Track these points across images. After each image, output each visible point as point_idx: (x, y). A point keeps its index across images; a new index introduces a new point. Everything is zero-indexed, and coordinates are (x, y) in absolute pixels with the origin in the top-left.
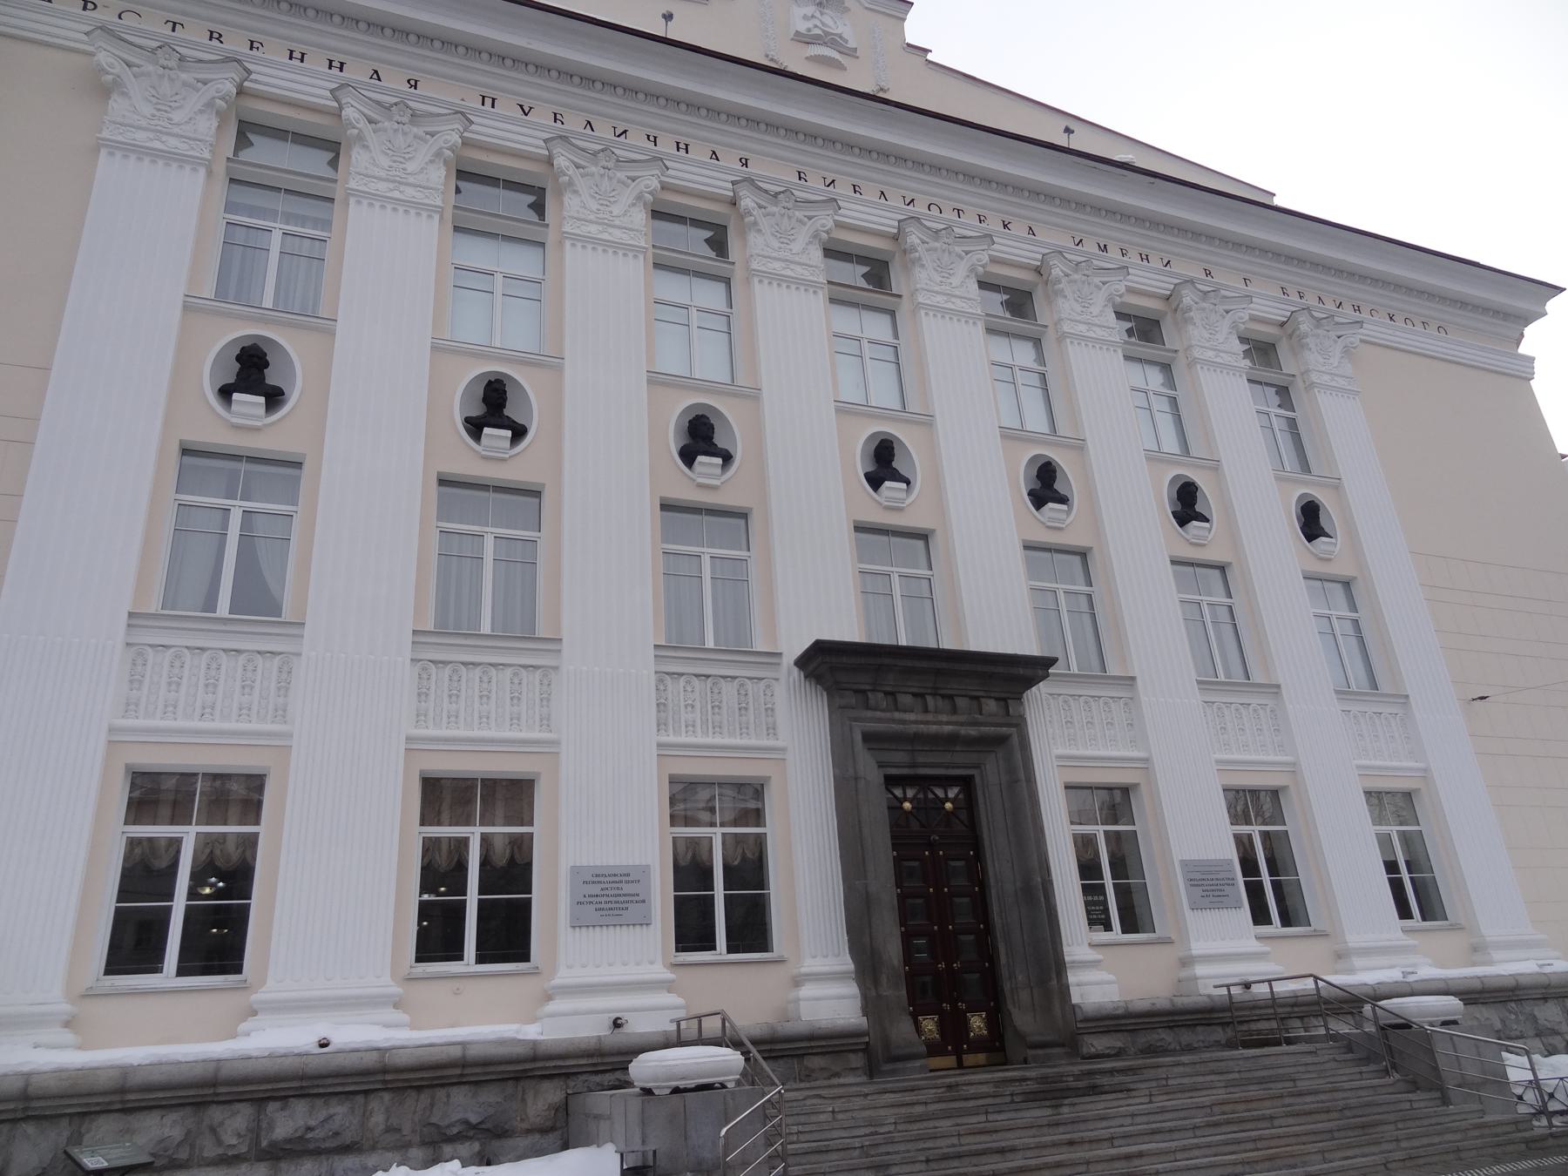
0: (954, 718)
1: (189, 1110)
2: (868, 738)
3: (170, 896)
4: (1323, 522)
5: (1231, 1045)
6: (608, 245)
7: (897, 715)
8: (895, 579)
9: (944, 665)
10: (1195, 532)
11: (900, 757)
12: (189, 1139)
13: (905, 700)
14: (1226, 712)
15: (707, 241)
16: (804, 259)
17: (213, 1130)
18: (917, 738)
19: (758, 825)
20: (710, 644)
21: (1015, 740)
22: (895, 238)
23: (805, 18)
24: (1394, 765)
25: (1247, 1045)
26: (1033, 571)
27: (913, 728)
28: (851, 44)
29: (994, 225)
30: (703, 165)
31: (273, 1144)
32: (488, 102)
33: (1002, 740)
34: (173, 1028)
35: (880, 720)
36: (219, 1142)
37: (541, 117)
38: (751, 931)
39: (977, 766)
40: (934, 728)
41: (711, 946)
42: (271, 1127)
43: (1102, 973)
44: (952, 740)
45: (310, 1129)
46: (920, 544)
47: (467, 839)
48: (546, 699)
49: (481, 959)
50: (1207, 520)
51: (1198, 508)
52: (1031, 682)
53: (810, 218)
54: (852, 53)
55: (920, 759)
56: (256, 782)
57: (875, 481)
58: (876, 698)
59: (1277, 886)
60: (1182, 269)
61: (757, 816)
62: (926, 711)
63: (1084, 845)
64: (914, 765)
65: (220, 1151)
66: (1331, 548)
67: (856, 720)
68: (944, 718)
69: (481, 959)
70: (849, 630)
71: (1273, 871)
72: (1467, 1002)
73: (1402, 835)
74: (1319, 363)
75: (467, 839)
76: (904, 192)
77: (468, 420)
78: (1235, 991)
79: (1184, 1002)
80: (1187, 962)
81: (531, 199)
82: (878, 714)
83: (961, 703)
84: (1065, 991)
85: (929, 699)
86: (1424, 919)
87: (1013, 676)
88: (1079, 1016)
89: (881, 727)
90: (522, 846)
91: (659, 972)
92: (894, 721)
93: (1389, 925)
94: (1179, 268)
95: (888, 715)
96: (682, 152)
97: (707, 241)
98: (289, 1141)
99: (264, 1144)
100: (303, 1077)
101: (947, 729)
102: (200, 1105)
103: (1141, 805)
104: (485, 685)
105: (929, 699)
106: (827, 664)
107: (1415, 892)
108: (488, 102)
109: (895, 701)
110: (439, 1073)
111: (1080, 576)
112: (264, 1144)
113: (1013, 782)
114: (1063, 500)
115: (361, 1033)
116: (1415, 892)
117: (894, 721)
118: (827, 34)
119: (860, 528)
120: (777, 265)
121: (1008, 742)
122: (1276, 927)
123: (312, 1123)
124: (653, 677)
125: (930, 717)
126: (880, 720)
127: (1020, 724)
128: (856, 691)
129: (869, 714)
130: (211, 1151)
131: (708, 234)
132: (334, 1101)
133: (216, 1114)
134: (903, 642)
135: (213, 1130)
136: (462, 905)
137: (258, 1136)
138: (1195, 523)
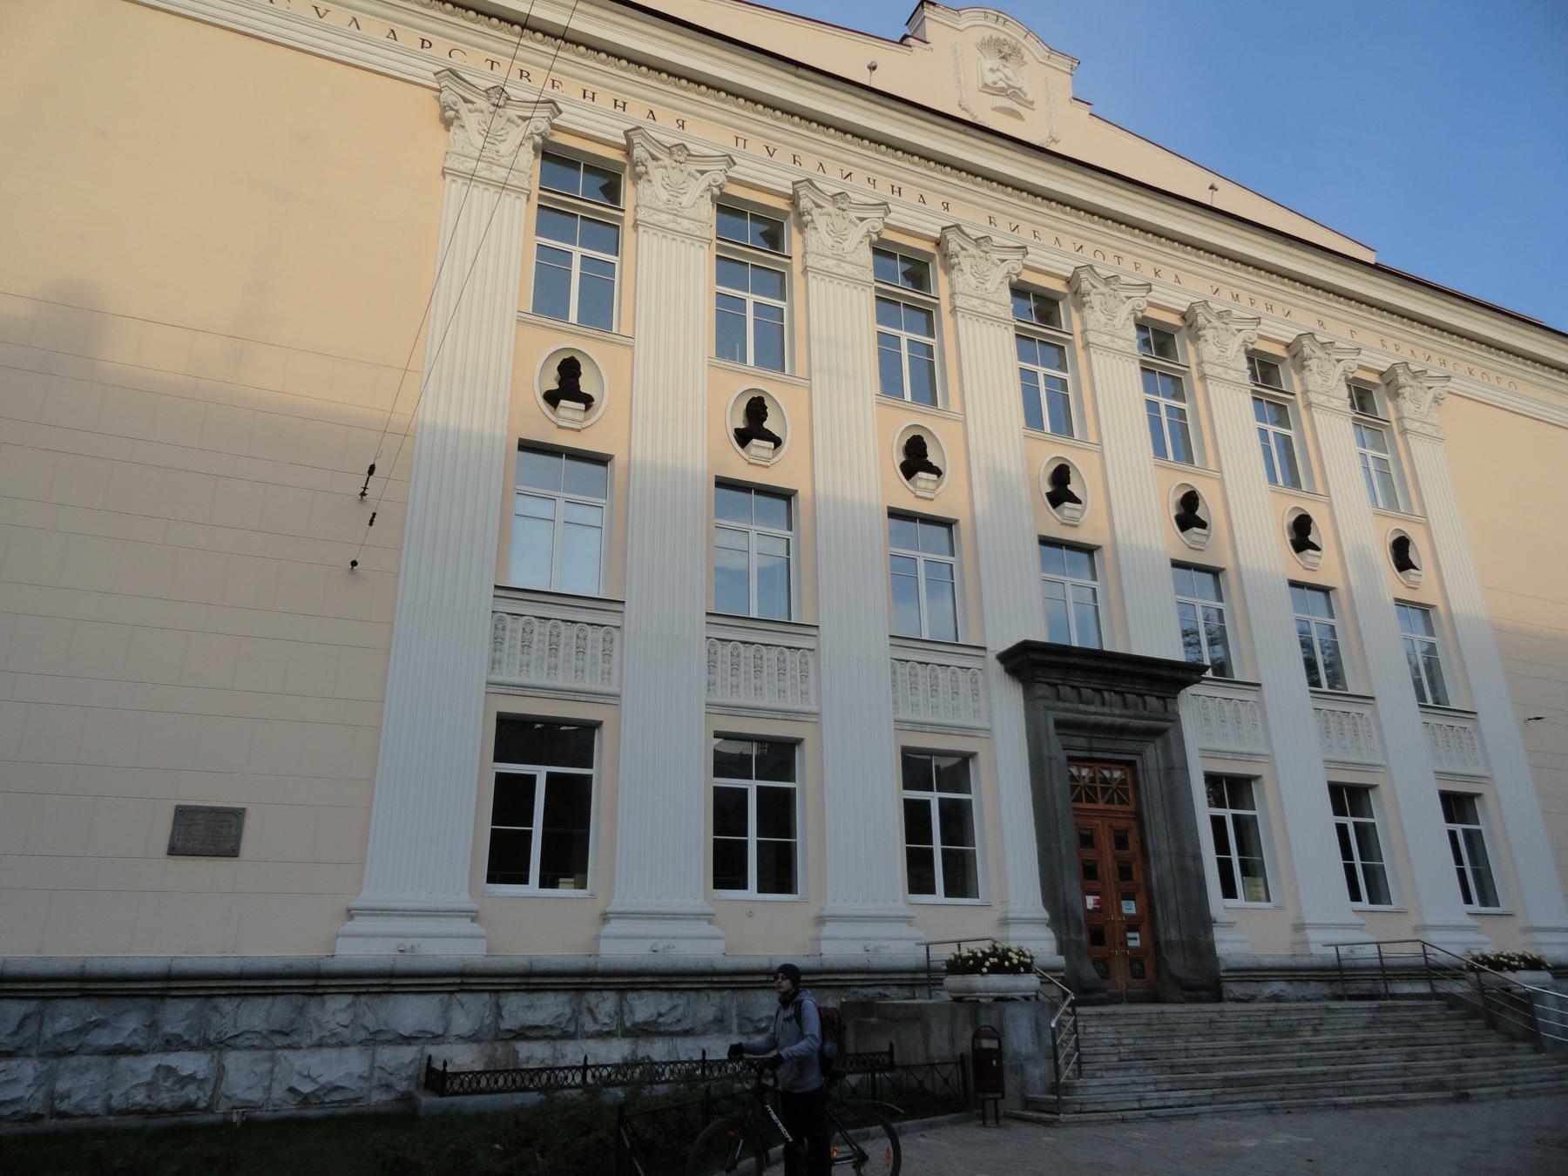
0: (1125, 712)
1: (573, 994)
2: (1060, 724)
3: (745, 833)
4: (1412, 556)
5: (1338, 998)
6: (842, 277)
7: (1082, 707)
8: (753, 535)
9: (1121, 667)
10: (1195, 537)
11: (1081, 742)
12: (575, 1017)
13: (1087, 693)
14: (1345, 721)
15: (762, 234)
16: (995, 298)
17: (591, 1012)
18: (1097, 727)
19: (788, 780)
20: (754, 614)
21: (1171, 734)
22: (1068, 281)
23: (992, 70)
24: (1463, 772)
25: (1351, 998)
26: (1046, 564)
27: (1093, 719)
28: (1030, 97)
29: (1260, 308)
30: (338, 32)
31: (635, 1025)
32: (741, 142)
33: (1161, 732)
34: (539, 924)
35: (1067, 710)
36: (596, 1020)
37: (784, 157)
38: (961, 881)
39: (1139, 754)
40: (1109, 720)
41: (932, 891)
42: (632, 1012)
43: (1243, 932)
44: (1123, 730)
45: (660, 1015)
46: (944, 530)
47: (534, 777)
48: (607, 654)
49: (762, 889)
50: (1318, 549)
51: (1311, 538)
52: (1186, 683)
53: (702, 172)
54: (1030, 104)
55: (1097, 745)
56: (588, 729)
57: (743, 438)
58: (1066, 691)
59: (1242, 862)
60: (809, 167)
61: (787, 771)
62: (1103, 704)
63: (1218, 823)
64: (1091, 750)
65: (597, 1027)
66: (1316, 560)
67: (1049, 708)
68: (1117, 712)
69: (760, 890)
70: (1040, 635)
71: (1241, 851)
72: (1555, 977)
73: (1355, 824)
74: (1413, 408)
75: (534, 777)
76: (893, 182)
77: (737, 431)
78: (1343, 950)
79: (1304, 961)
80: (1299, 927)
81: (603, 182)
82: (1068, 705)
83: (1131, 698)
84: (1211, 947)
85: (1106, 694)
86: (1372, 902)
87: (1166, 679)
88: (1223, 967)
89: (1070, 716)
90: (787, 797)
91: (463, 900)
92: (1078, 711)
93: (1457, 911)
94: (1297, 315)
95: (1074, 706)
96: (588, 100)
97: (762, 234)
98: (646, 1023)
99: (628, 1024)
100: (868, 971)
101: (1119, 721)
102: (581, 990)
103: (804, 762)
104: (527, 636)
105: (1106, 694)
106: (1026, 662)
107: (1478, 882)
108: (741, 142)
109: (1079, 694)
110: (243, 983)
111: (1211, 591)
112: (628, 1024)
113: (1170, 769)
114: (1203, 525)
115: (1320, 947)
116: (1478, 882)
117: (1078, 711)
118: (1010, 87)
119: (1045, 541)
120: (975, 302)
121: (1164, 731)
122: (1365, 904)
123: (663, 1010)
124: (705, 645)
125: (1106, 710)
126: (1067, 710)
127: (1176, 719)
128: (1050, 684)
129: (1061, 704)
130: (590, 1027)
131: (764, 228)
132: (676, 994)
133: (592, 998)
134: (1075, 643)
135: (591, 1012)
136: (931, 851)
137: (622, 1019)
138: (1067, 504)
